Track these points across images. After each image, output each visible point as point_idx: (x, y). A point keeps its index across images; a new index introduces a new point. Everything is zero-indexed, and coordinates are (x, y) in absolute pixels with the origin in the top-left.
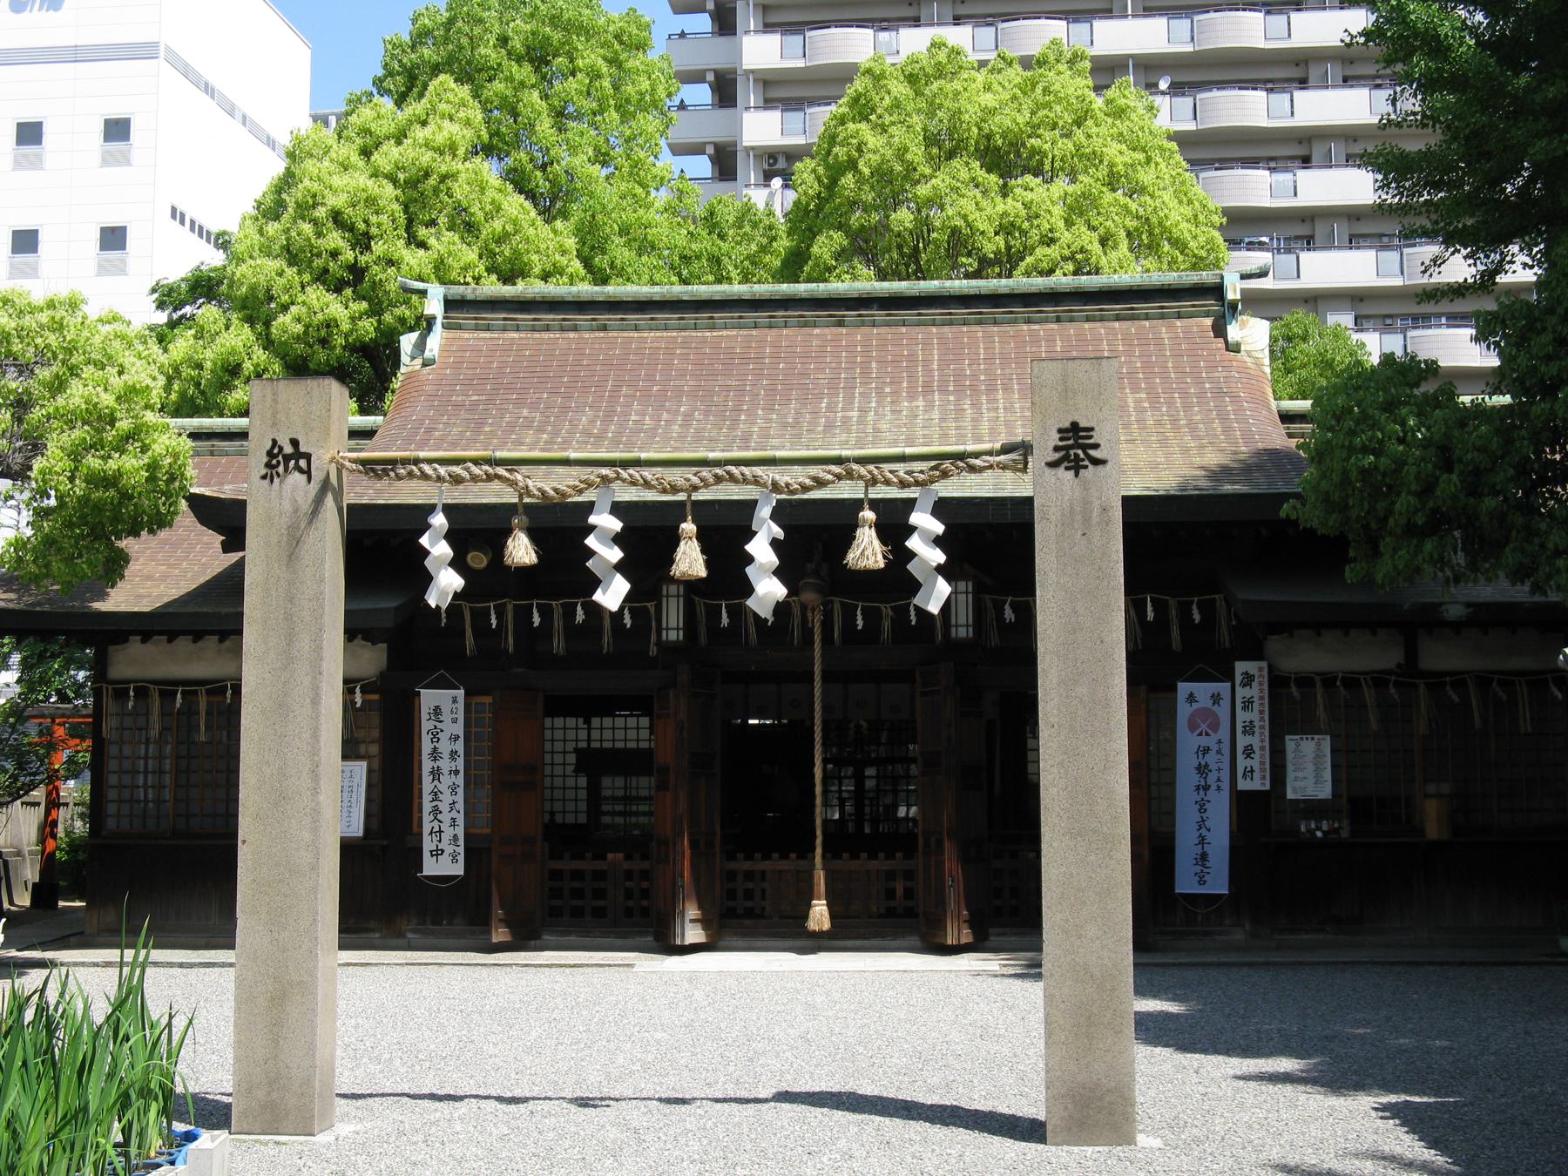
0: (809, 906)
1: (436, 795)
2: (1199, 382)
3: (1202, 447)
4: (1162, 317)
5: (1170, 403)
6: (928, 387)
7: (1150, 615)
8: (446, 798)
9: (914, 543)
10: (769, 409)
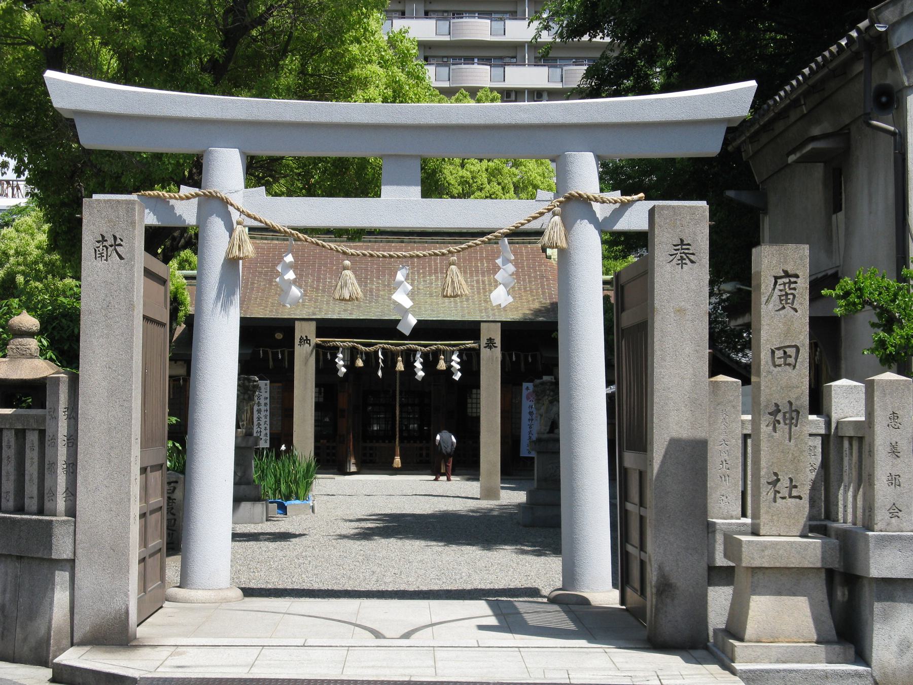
0: (393, 459)
1: (259, 419)
2: (535, 272)
3: (534, 300)
4: (523, 243)
5: (524, 280)
6: (436, 270)
7: (514, 359)
8: (263, 420)
9: (453, 363)
10: (378, 278)
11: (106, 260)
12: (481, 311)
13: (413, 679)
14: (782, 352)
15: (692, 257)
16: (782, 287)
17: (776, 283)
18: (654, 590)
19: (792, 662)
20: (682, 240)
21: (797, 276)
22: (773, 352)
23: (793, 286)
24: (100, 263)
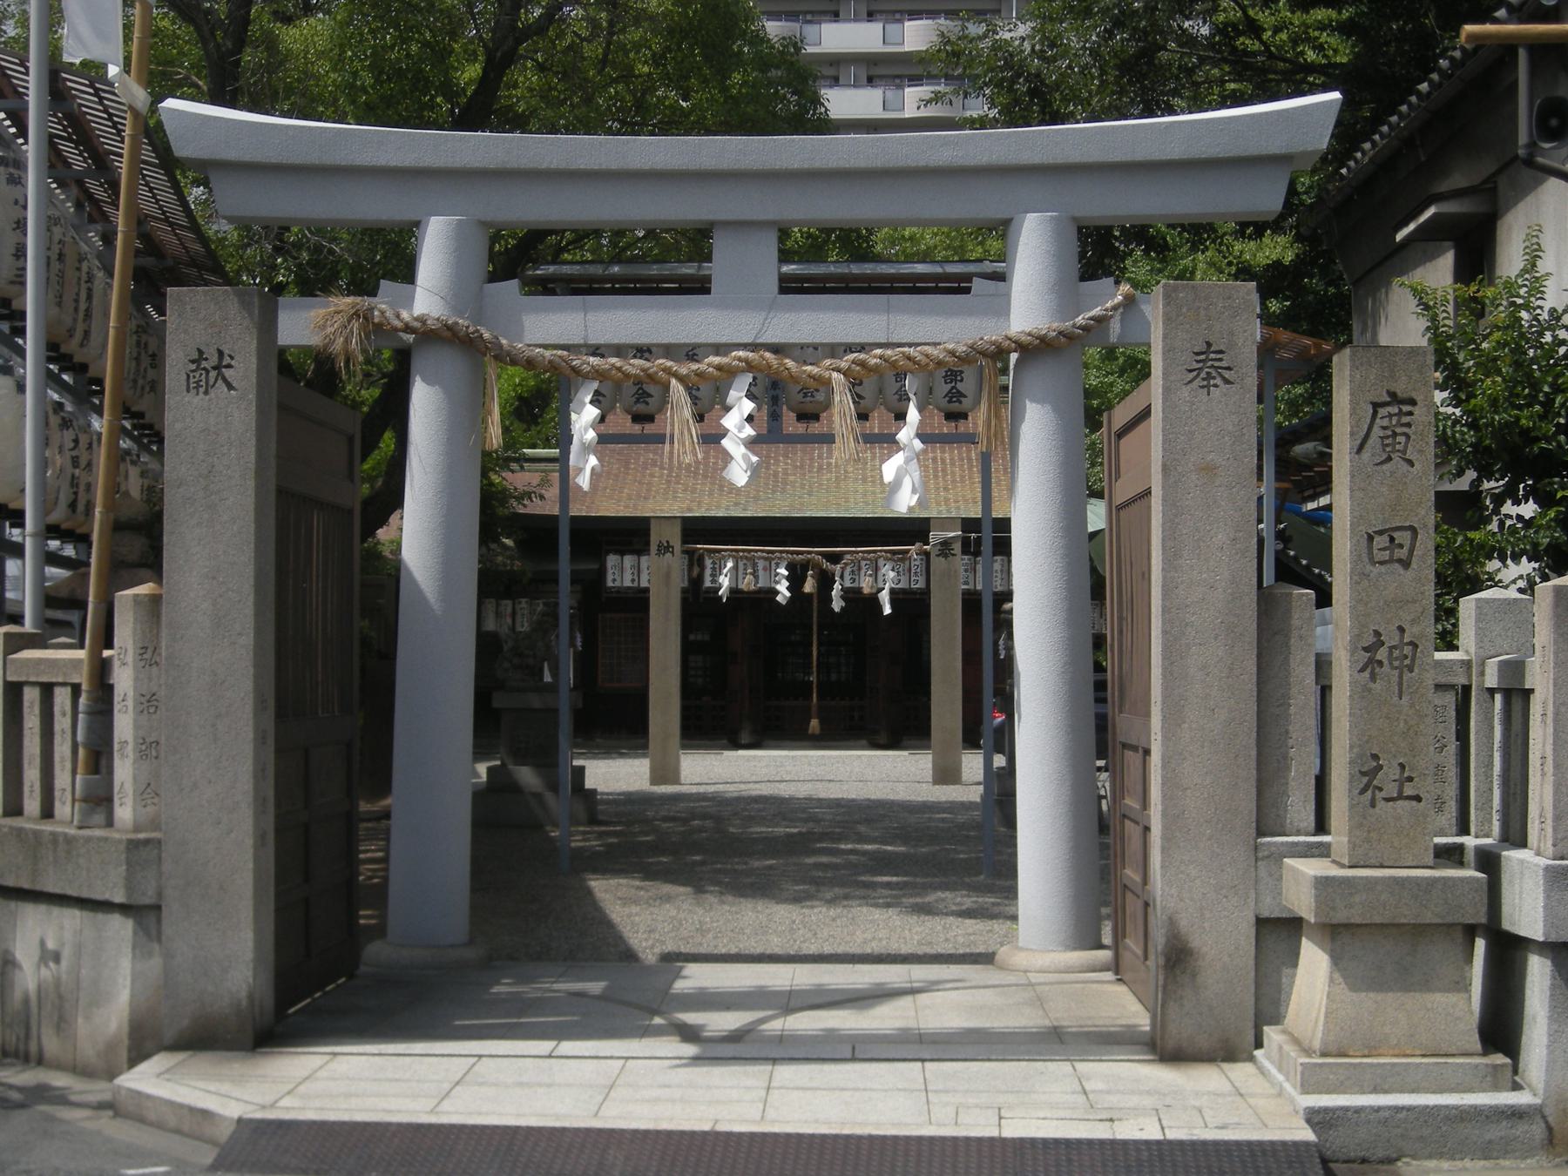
11: (206, 393)
12: (938, 504)
13: (722, 1128)
14: (1386, 538)
15: (1227, 374)
16: (1385, 422)
17: (1375, 413)
18: (1161, 961)
19: (1402, 1091)
20: (1209, 344)
21: (1413, 402)
22: (1370, 538)
23: (1405, 420)
24: (198, 400)
